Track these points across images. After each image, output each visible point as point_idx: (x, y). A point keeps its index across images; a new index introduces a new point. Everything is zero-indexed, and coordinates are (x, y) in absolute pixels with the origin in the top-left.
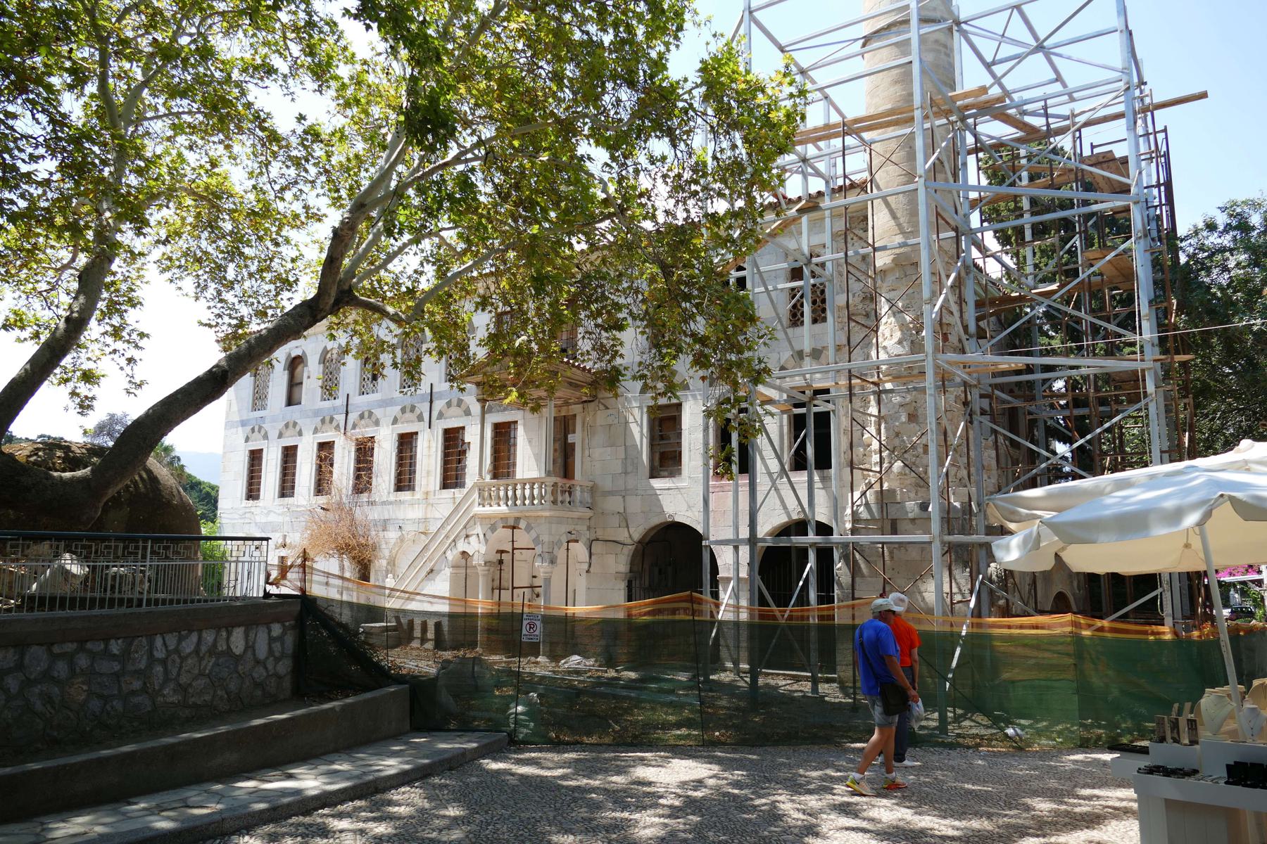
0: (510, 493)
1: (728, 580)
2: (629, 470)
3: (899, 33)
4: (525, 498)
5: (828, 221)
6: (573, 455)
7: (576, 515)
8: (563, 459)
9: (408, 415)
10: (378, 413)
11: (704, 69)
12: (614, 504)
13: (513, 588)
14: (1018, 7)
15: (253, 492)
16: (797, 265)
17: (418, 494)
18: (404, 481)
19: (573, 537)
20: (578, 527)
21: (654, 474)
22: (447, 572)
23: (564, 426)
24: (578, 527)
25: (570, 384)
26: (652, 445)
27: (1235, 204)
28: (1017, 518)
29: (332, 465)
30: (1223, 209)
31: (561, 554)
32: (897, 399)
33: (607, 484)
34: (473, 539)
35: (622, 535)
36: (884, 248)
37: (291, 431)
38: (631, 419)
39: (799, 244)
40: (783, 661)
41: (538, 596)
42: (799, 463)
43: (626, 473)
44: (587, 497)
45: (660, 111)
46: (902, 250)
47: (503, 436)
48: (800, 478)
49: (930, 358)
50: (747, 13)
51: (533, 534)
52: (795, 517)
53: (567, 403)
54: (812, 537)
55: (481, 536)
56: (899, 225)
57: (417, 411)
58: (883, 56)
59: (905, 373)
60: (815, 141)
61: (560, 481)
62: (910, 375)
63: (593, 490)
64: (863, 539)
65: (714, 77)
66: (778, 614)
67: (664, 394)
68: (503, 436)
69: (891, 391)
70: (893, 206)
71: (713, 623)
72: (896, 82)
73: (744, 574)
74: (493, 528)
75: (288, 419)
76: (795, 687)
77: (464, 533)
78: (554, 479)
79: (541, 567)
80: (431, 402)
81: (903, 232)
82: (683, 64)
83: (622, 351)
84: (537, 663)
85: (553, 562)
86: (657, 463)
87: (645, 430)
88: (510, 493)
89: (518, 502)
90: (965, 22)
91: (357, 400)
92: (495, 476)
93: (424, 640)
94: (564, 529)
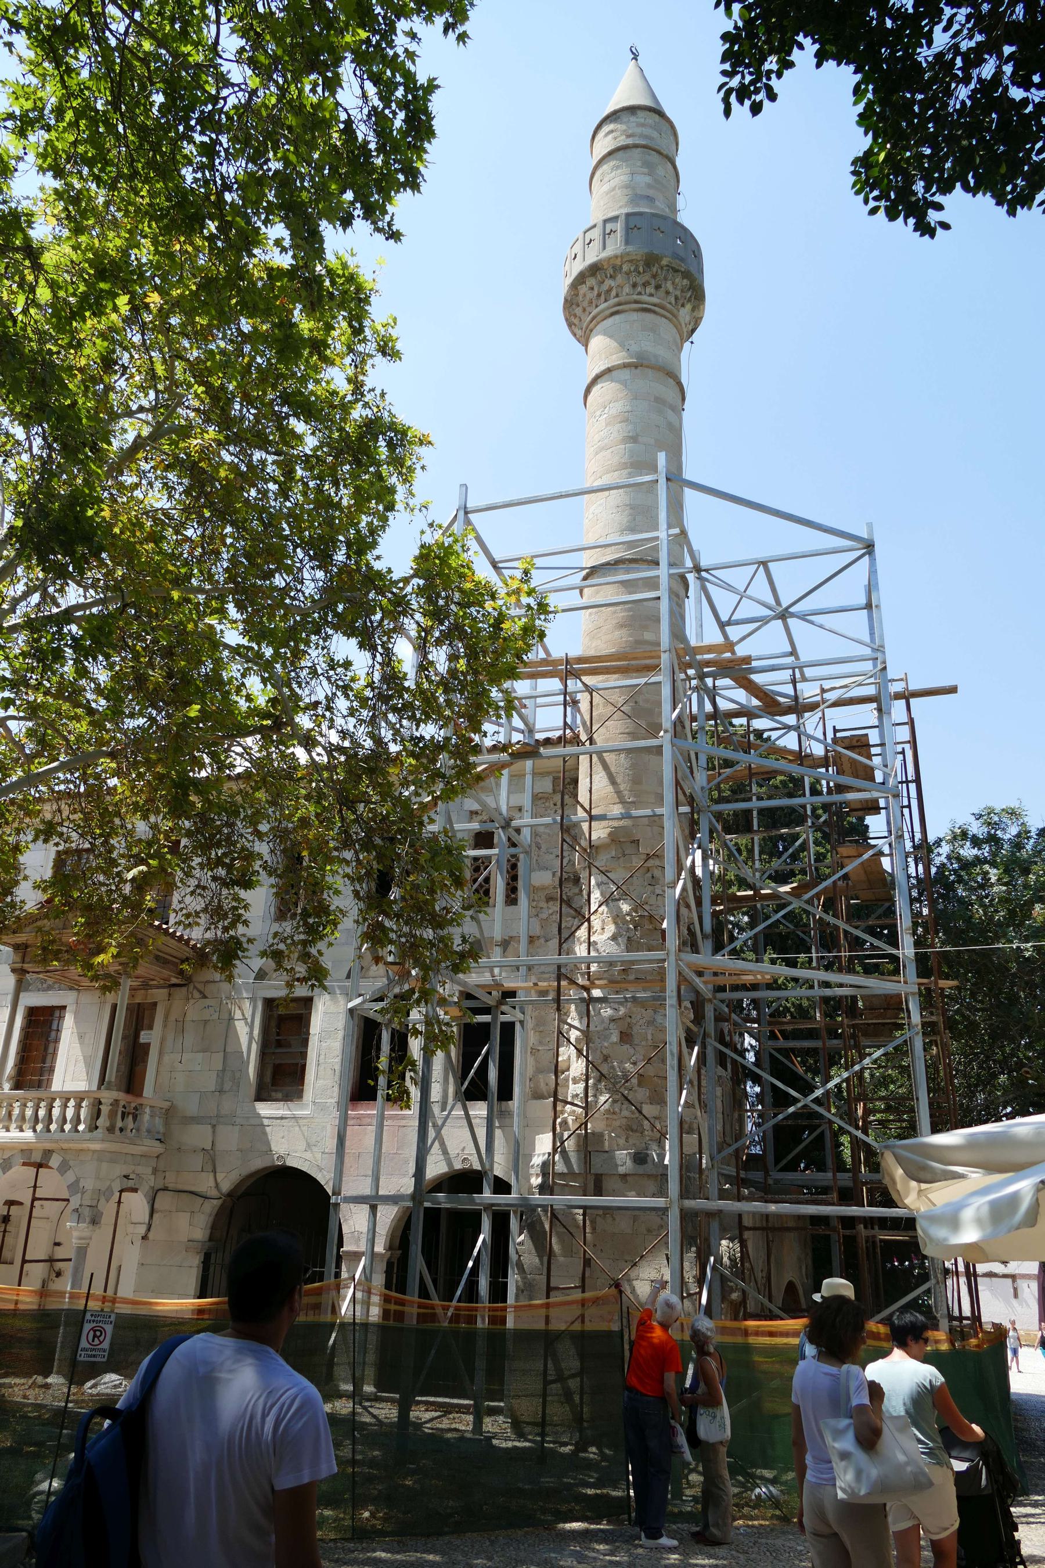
0: (42, 1113)
1: (356, 1256)
2: (227, 1087)
3: (628, 571)
4: (65, 1121)
5: (529, 779)
7: (137, 1150)
8: (127, 1066)
11: (425, 555)
12: (198, 1136)
13: (24, 1261)
14: (764, 564)
16: (489, 827)
19: (130, 1184)
20: (140, 1170)
21: (261, 1096)
23: (140, 1017)
24: (140, 1170)
25: (157, 958)
26: (263, 1054)
27: (991, 811)
28: (929, 1177)
30: (978, 817)
31: (108, 1210)
32: (607, 1012)
33: (191, 1106)
35: (205, 1184)
36: (602, 818)
38: (238, 1015)
39: (497, 802)
40: (444, 1380)
41: (59, 1274)
42: (475, 1091)
43: (221, 1092)
44: (159, 1123)
45: (357, 601)
46: (621, 823)
48: (479, 1110)
49: (672, 958)
50: (461, 513)
51: (70, 1177)
52: (458, 1166)
53: (146, 986)
54: (487, 1195)
56: (618, 793)
58: (606, 592)
59: (619, 978)
60: (533, 676)
61: (121, 1096)
62: (625, 981)
63: (169, 1113)
64: (559, 1200)
65: (436, 566)
66: (439, 1311)
67: (304, 980)
69: (599, 1000)
70: (613, 769)
71: (332, 1325)
72: (621, 626)
73: (379, 1248)
76: (445, 1424)
79: (74, 1231)
81: (622, 802)
82: (396, 553)
83: (247, 915)
84: (47, 1386)
85: (95, 1221)
87: (256, 1032)
88: (42, 1113)
89: (53, 1127)
90: (707, 571)
92: (17, 1086)
94: (120, 1170)
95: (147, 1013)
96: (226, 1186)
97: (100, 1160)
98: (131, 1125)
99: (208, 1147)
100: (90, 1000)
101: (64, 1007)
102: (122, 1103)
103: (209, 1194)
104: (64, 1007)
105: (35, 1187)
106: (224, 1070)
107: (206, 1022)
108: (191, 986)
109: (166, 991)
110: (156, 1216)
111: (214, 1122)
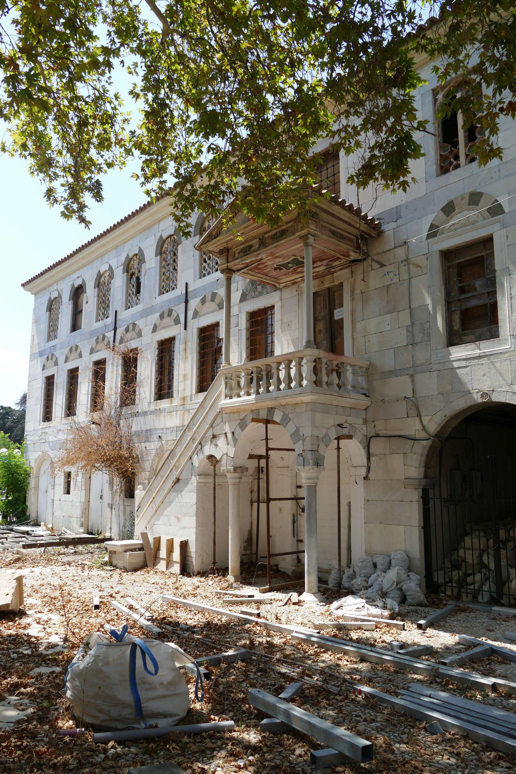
2: (418, 339)
6: (341, 334)
8: (328, 333)
9: (167, 320)
10: (140, 323)
12: (400, 386)
15: (47, 416)
17: (176, 401)
18: (164, 390)
19: (345, 432)
20: (351, 420)
21: (453, 339)
22: (194, 480)
24: (351, 420)
29: (104, 381)
31: (329, 455)
33: (388, 362)
34: (221, 441)
35: (413, 428)
37: (75, 355)
44: (362, 381)
47: (259, 324)
51: (291, 427)
55: (230, 435)
57: (174, 315)
63: (369, 371)
68: (259, 324)
74: (243, 425)
75: (72, 344)
77: (210, 435)
78: (316, 352)
79: (305, 475)
80: (186, 302)
85: (318, 463)
86: (457, 326)
91: (125, 315)
93: (169, 563)
94: (333, 420)
95: (336, 294)
96: (433, 428)
97: (313, 411)
98: (336, 381)
99: (410, 394)
100: (289, 294)
101: (273, 307)
102: (324, 360)
103: (417, 436)
104: (273, 307)
105: (267, 439)
106: (412, 324)
107: (388, 286)
108: (369, 259)
109: (348, 270)
110: (372, 459)
111: (411, 372)
